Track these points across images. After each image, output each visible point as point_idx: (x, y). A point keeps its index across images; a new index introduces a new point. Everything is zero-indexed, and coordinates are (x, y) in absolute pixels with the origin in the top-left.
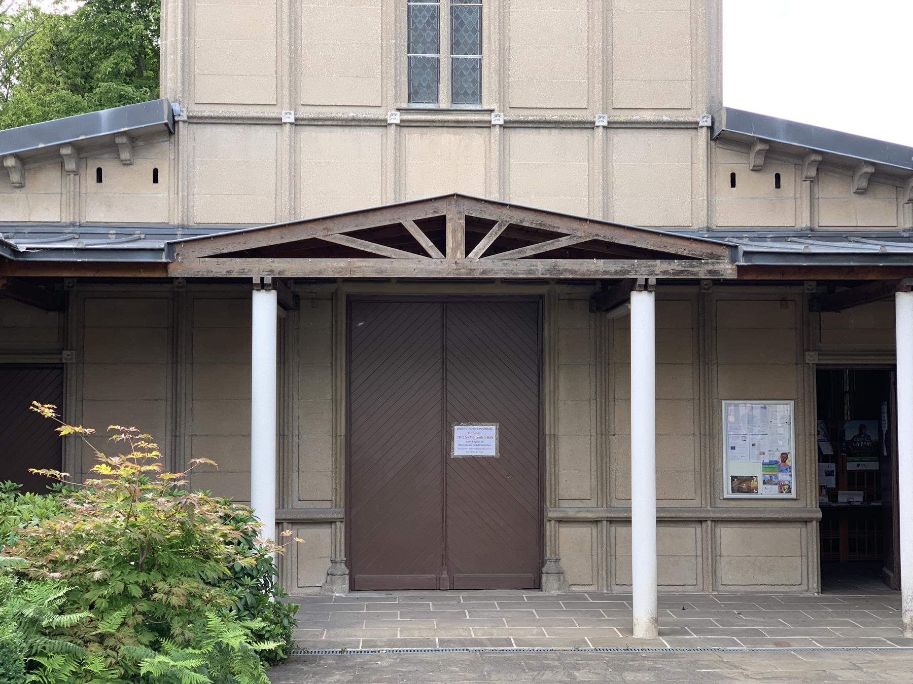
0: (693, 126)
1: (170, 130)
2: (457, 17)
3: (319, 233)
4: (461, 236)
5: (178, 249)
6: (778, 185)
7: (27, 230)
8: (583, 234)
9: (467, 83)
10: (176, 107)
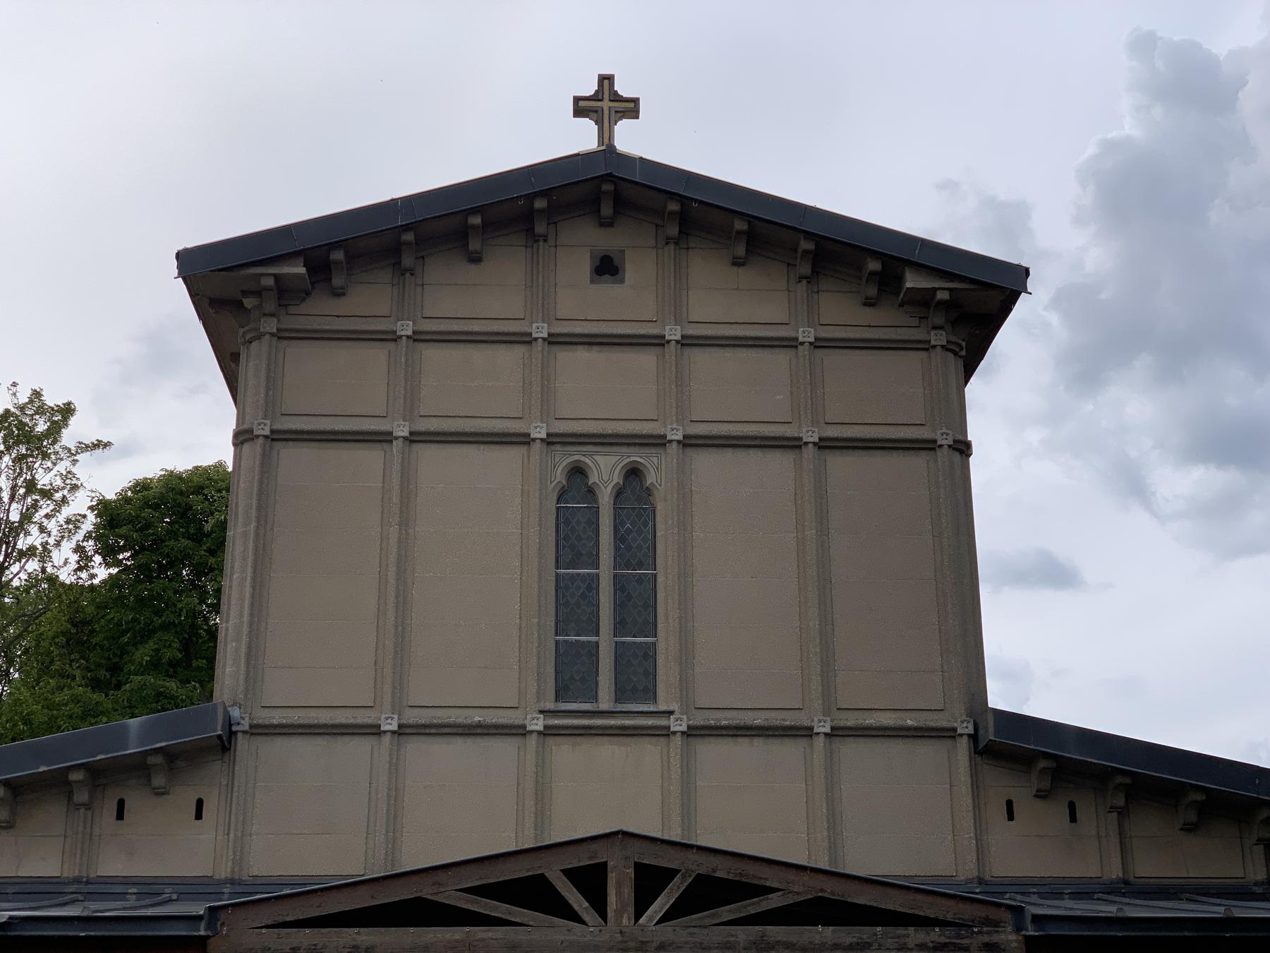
0: (948, 734)
1: (224, 745)
2: (623, 589)
3: (427, 892)
4: (628, 892)
5: (223, 916)
6: (1073, 819)
7: (11, 889)
8: (802, 890)
9: (637, 676)
10: (235, 713)
